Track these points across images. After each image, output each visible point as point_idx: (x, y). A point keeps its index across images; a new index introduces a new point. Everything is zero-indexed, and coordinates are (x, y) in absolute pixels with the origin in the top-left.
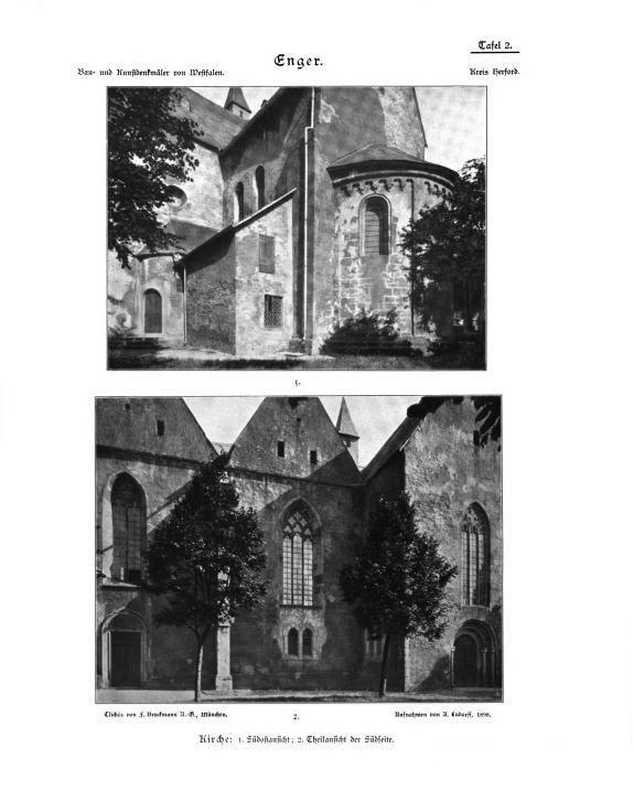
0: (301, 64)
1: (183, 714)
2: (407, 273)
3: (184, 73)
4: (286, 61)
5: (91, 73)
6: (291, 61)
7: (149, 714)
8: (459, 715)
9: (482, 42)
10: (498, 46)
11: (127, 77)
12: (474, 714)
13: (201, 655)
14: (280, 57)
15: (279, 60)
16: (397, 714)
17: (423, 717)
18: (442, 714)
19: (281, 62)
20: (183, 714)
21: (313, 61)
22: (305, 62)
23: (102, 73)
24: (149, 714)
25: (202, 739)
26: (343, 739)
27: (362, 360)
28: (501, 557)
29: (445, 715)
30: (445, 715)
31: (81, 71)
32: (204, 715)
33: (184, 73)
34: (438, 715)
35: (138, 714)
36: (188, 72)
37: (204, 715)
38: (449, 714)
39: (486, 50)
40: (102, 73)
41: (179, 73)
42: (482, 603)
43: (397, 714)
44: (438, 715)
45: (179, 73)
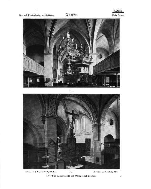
0: (72, 15)
1: (45, 172)
2: (85, 68)
3: (44, 15)
4: (69, 15)
7: (37, 172)
9: (115, 10)
10: (119, 11)
12: (107, 172)
14: (67, 14)
16: (94, 172)
20: (45, 172)
21: (75, 15)
22: (73, 15)
23: (25, 15)
24: (37, 172)
25: (48, 176)
26: (76, 176)
32: (50, 172)
33: (44, 15)
34: (34, 172)
35: (35, 172)
36: (45, 15)
38: (36, 172)
39: (116, 12)
40: (25, 15)
41: (43, 15)
42: (39, 135)
43: (94, 172)
44: (34, 172)
45: (43, 15)
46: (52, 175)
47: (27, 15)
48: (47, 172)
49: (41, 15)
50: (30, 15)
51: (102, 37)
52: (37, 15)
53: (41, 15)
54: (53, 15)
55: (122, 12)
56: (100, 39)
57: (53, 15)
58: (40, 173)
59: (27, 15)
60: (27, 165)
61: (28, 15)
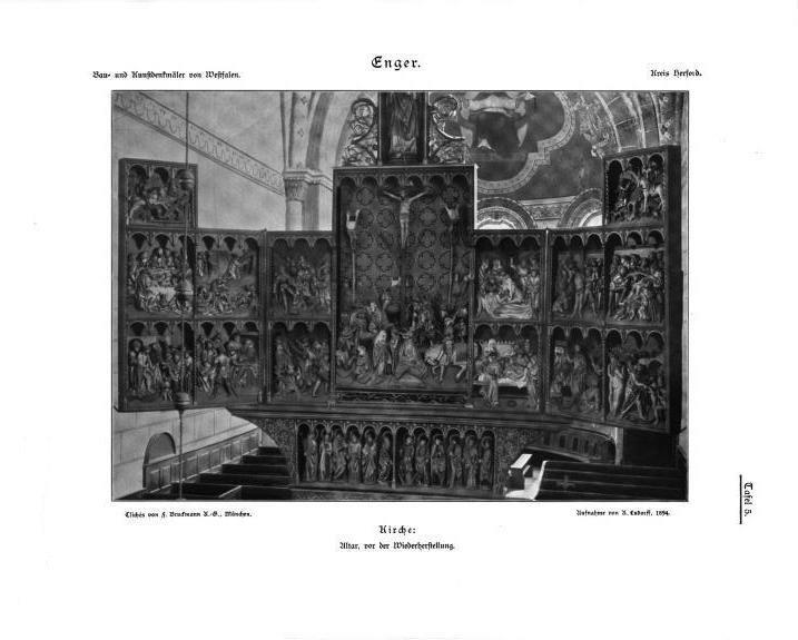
0: (398, 66)
4: (383, 63)
5: (106, 76)
6: (388, 63)
7: (172, 514)
8: (234, 514)
11: (143, 79)
12: (653, 512)
13: (598, 483)
14: (377, 60)
15: (376, 62)
16: (580, 513)
17: (246, 517)
18: (202, 514)
19: (379, 64)
21: (411, 63)
22: (402, 64)
23: (117, 76)
24: (172, 514)
27: (685, 296)
28: (687, 420)
29: (206, 514)
30: (206, 514)
31: (344, 546)
32: (228, 514)
35: (160, 515)
37: (228, 514)
38: (168, 514)
39: (743, 490)
40: (117, 76)
41: (195, 75)
43: (580, 513)
45: (195, 75)
46: (398, 528)
47: (124, 75)
48: (215, 514)
49: (187, 75)
50: (140, 76)
51: (190, 112)
52: (227, 76)
53: (187, 75)
54: (236, 75)
55: (743, 514)
56: (297, 113)
57: (236, 75)
58: (589, 516)
59: (124, 75)
60: (675, 488)
61: (130, 74)
